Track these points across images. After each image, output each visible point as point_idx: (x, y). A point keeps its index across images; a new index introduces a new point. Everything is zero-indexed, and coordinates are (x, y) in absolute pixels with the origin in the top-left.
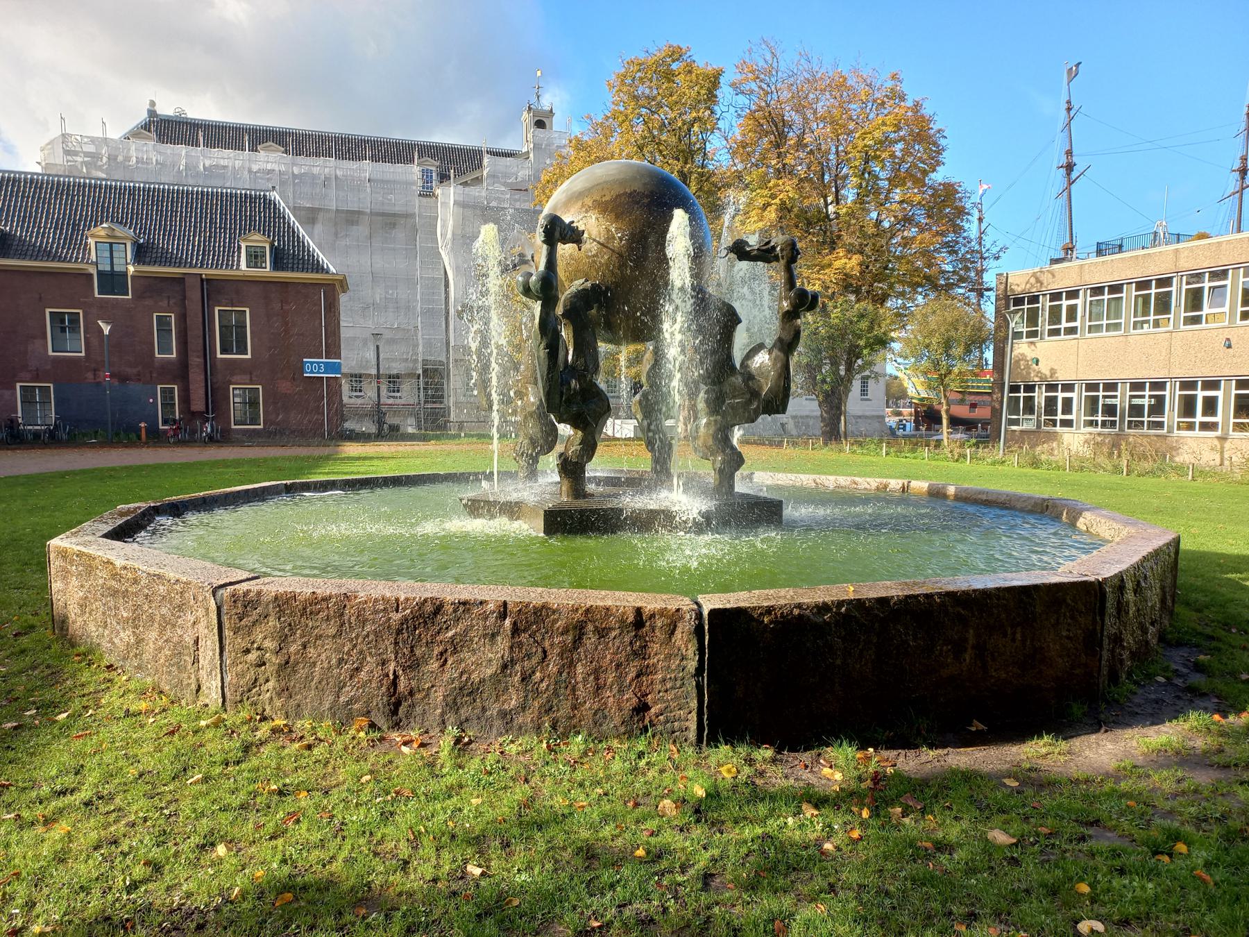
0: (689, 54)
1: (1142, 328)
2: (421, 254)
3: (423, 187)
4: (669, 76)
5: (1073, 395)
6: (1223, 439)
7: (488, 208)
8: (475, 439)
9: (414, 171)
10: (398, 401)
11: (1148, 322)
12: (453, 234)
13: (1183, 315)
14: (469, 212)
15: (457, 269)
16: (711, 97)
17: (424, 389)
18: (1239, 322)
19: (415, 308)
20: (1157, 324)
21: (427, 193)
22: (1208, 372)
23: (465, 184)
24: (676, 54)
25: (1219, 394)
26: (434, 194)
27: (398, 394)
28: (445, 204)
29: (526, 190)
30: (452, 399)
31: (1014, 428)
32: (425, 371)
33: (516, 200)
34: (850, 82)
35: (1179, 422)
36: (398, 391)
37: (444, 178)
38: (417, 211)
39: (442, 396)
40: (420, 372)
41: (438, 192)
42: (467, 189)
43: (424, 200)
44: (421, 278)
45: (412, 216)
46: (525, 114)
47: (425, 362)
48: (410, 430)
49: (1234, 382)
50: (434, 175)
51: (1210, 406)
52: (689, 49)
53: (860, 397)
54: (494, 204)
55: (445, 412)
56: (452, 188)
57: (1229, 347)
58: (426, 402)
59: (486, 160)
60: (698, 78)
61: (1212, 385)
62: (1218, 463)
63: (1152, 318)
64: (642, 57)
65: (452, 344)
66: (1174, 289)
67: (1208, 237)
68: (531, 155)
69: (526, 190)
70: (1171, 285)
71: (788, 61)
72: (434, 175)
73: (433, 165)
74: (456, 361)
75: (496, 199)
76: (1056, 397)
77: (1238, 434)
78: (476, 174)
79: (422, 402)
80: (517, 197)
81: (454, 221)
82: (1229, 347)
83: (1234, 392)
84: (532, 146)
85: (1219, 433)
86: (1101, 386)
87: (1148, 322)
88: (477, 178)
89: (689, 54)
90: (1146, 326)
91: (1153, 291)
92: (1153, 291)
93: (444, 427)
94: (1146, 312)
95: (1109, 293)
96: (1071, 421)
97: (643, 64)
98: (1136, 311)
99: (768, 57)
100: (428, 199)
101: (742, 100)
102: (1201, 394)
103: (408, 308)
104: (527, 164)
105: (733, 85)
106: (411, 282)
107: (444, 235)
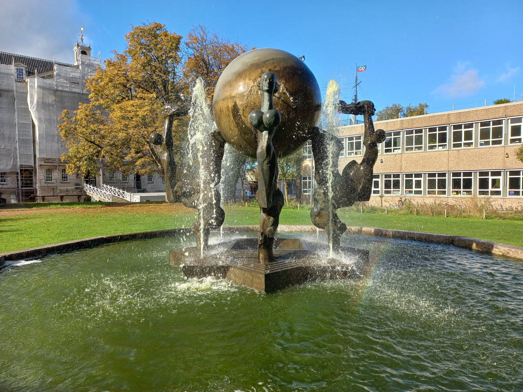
0: (164, 28)
1: (351, 155)
2: (18, 111)
3: (18, 77)
4: (156, 36)
5: (422, 179)
6: (381, 197)
7: (57, 90)
8: (59, 206)
9: (12, 68)
10: (5, 186)
11: (353, 152)
12: (37, 102)
13: (428, 145)
14: (46, 92)
15: (40, 120)
16: (177, 48)
17: (21, 180)
18: (385, 153)
19: (15, 138)
20: (356, 153)
21: (20, 80)
22: (418, 171)
23: (44, 78)
24: (158, 27)
25: (422, 179)
26: (24, 81)
27: (5, 183)
28: (32, 87)
29: (78, 83)
30: (38, 185)
31: (305, 194)
32: (21, 170)
33: (72, 88)
34: (235, 49)
35: (509, 191)
36: (5, 181)
37: (30, 73)
38: (15, 89)
39: (32, 184)
40: (19, 171)
41: (28, 80)
42: (45, 80)
43: (19, 84)
44: (18, 123)
45: (12, 91)
46: (76, 48)
47: (21, 166)
48: (13, 201)
49: (478, 173)
50: (24, 72)
51: (495, 183)
52: (165, 25)
53: (162, 182)
54: (60, 88)
55: (34, 192)
56: (36, 79)
57: (382, 162)
58: (22, 187)
59: (55, 67)
60: (171, 39)
61: (418, 175)
62: (380, 206)
63: (354, 151)
64: (142, 26)
65: (38, 156)
66: (447, 131)
67: (508, 101)
68: (80, 67)
69: (78, 83)
70: (400, 135)
71: (210, 37)
72: (24, 72)
73: (23, 67)
74: (40, 165)
75: (61, 86)
76: (412, 180)
77: (387, 195)
78: (50, 73)
79: (20, 187)
80: (73, 86)
81: (38, 95)
82: (382, 162)
83: (427, 178)
84: (80, 63)
85: (380, 194)
86: (490, 173)
87: (353, 152)
88: (50, 75)
89: (164, 28)
90: (352, 154)
91: (354, 141)
92: (354, 141)
93: (33, 199)
94: (352, 149)
95: (394, 135)
96: (421, 191)
97: (143, 29)
98: (349, 149)
99: (202, 33)
100: (22, 84)
101: (191, 51)
102: (490, 178)
103: (10, 138)
104: (78, 71)
105: (187, 44)
106: (12, 125)
107: (32, 102)
